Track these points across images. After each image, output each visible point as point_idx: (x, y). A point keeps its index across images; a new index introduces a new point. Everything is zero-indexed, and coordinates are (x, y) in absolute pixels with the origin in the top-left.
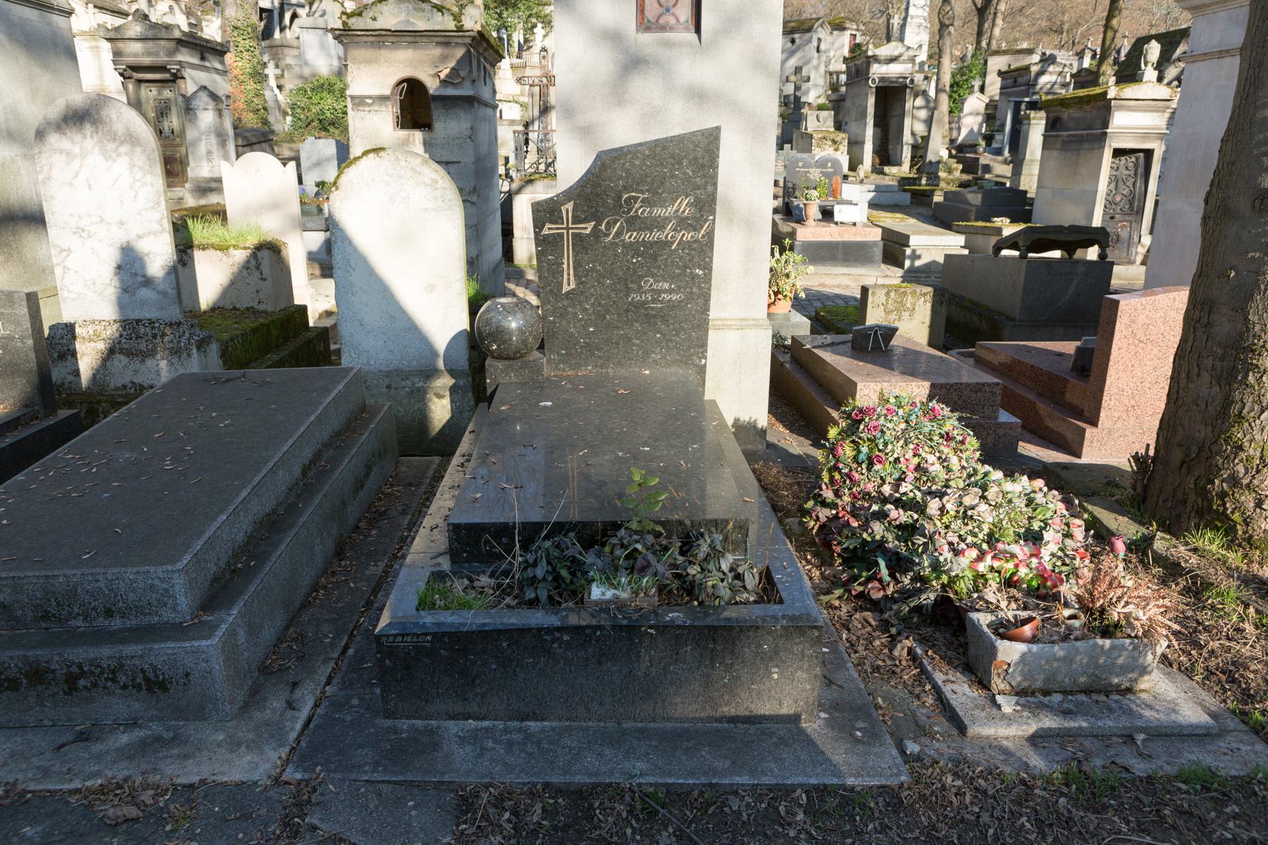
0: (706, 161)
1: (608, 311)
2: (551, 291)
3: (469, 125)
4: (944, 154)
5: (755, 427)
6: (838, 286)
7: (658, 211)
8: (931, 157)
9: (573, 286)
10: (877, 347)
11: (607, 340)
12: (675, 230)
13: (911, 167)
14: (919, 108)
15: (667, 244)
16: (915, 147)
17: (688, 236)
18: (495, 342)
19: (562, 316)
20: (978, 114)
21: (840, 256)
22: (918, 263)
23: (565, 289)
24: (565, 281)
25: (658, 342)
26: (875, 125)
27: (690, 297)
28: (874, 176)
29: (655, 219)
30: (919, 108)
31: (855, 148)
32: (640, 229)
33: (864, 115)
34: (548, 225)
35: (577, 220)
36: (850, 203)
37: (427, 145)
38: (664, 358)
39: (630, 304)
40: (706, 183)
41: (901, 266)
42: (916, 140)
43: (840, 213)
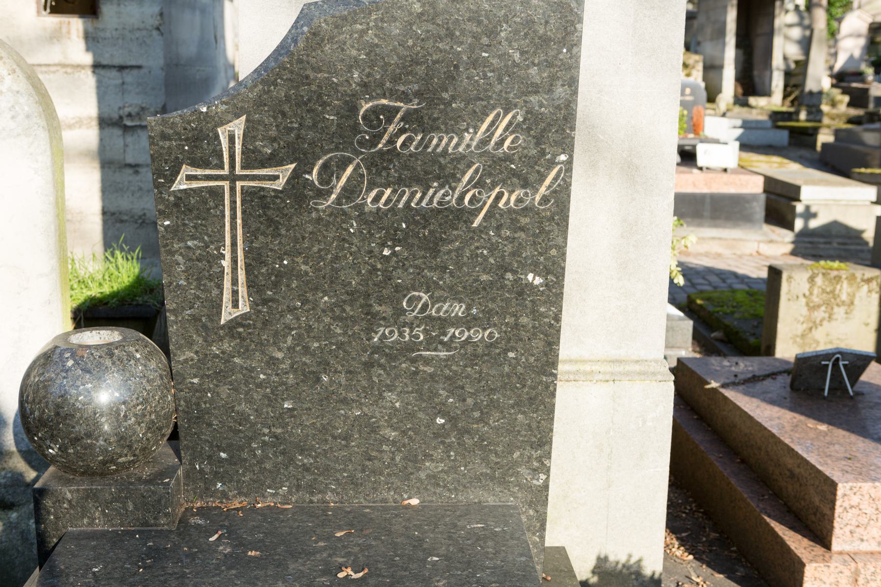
0: (552, 30)
1: (325, 365)
2: (195, 319)
3: (156, 9)
4: (826, 83)
5: (638, 574)
6: (707, 255)
7: (440, 142)
8: (811, 85)
9: (244, 307)
10: (838, 387)
11: (324, 429)
12: (480, 184)
13: (785, 97)
14: (790, 26)
15: (460, 216)
16: (788, 74)
17: (510, 199)
18: (53, 438)
19: (220, 376)
20: (859, 36)
21: (707, 214)
22: (814, 224)
23: (227, 314)
24: (227, 296)
25: (440, 434)
26: (738, 46)
27: (514, 336)
28: (737, 109)
29: (434, 158)
30: (790, 26)
31: (712, 74)
32: (400, 182)
33: (721, 33)
34: (186, 170)
35: (252, 159)
36: (717, 142)
37: (91, 40)
38: (454, 469)
39: (377, 349)
40: (553, 78)
41: (790, 226)
42: (787, 65)
43: (705, 155)
